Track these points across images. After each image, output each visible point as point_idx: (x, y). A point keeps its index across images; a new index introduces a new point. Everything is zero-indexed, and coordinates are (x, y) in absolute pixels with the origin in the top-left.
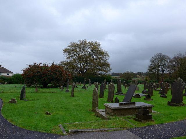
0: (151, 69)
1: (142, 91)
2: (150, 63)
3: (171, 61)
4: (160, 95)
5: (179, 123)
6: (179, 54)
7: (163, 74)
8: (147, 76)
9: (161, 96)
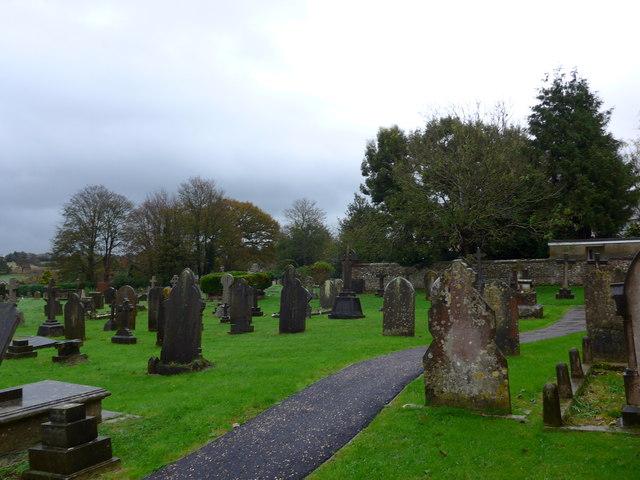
0: (66, 239)
1: (41, 328)
2: (64, 219)
3: (136, 215)
4: (113, 334)
5: (222, 451)
6: (159, 192)
7: (108, 259)
8: (53, 265)
9: (115, 341)
